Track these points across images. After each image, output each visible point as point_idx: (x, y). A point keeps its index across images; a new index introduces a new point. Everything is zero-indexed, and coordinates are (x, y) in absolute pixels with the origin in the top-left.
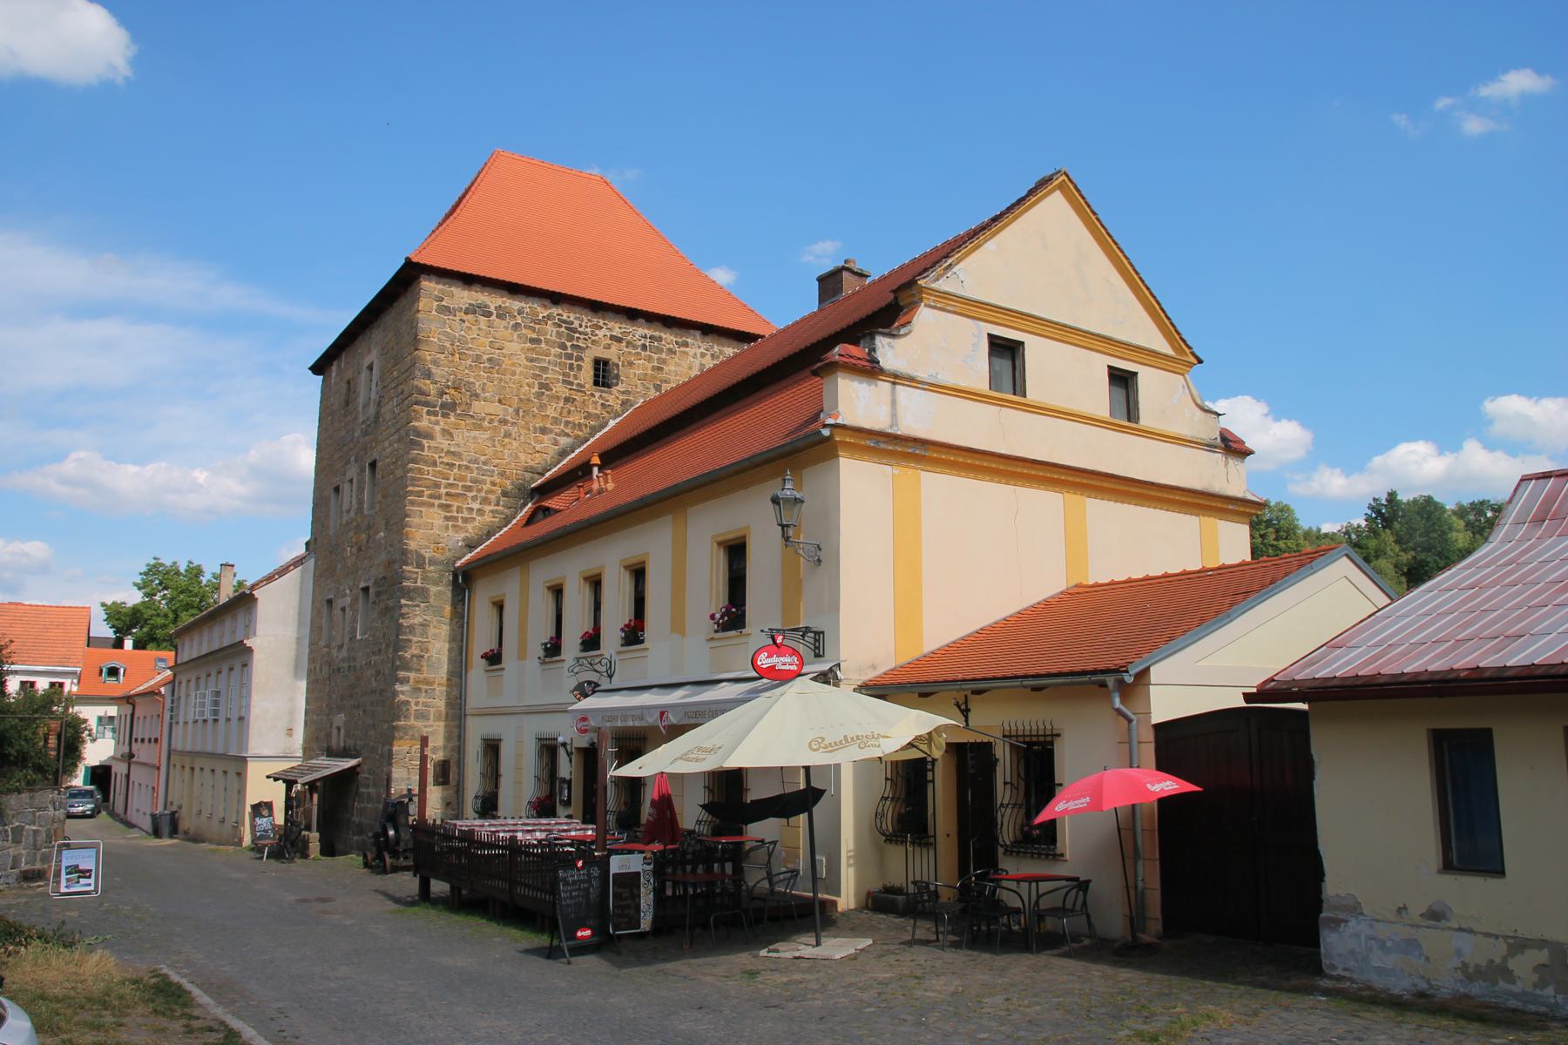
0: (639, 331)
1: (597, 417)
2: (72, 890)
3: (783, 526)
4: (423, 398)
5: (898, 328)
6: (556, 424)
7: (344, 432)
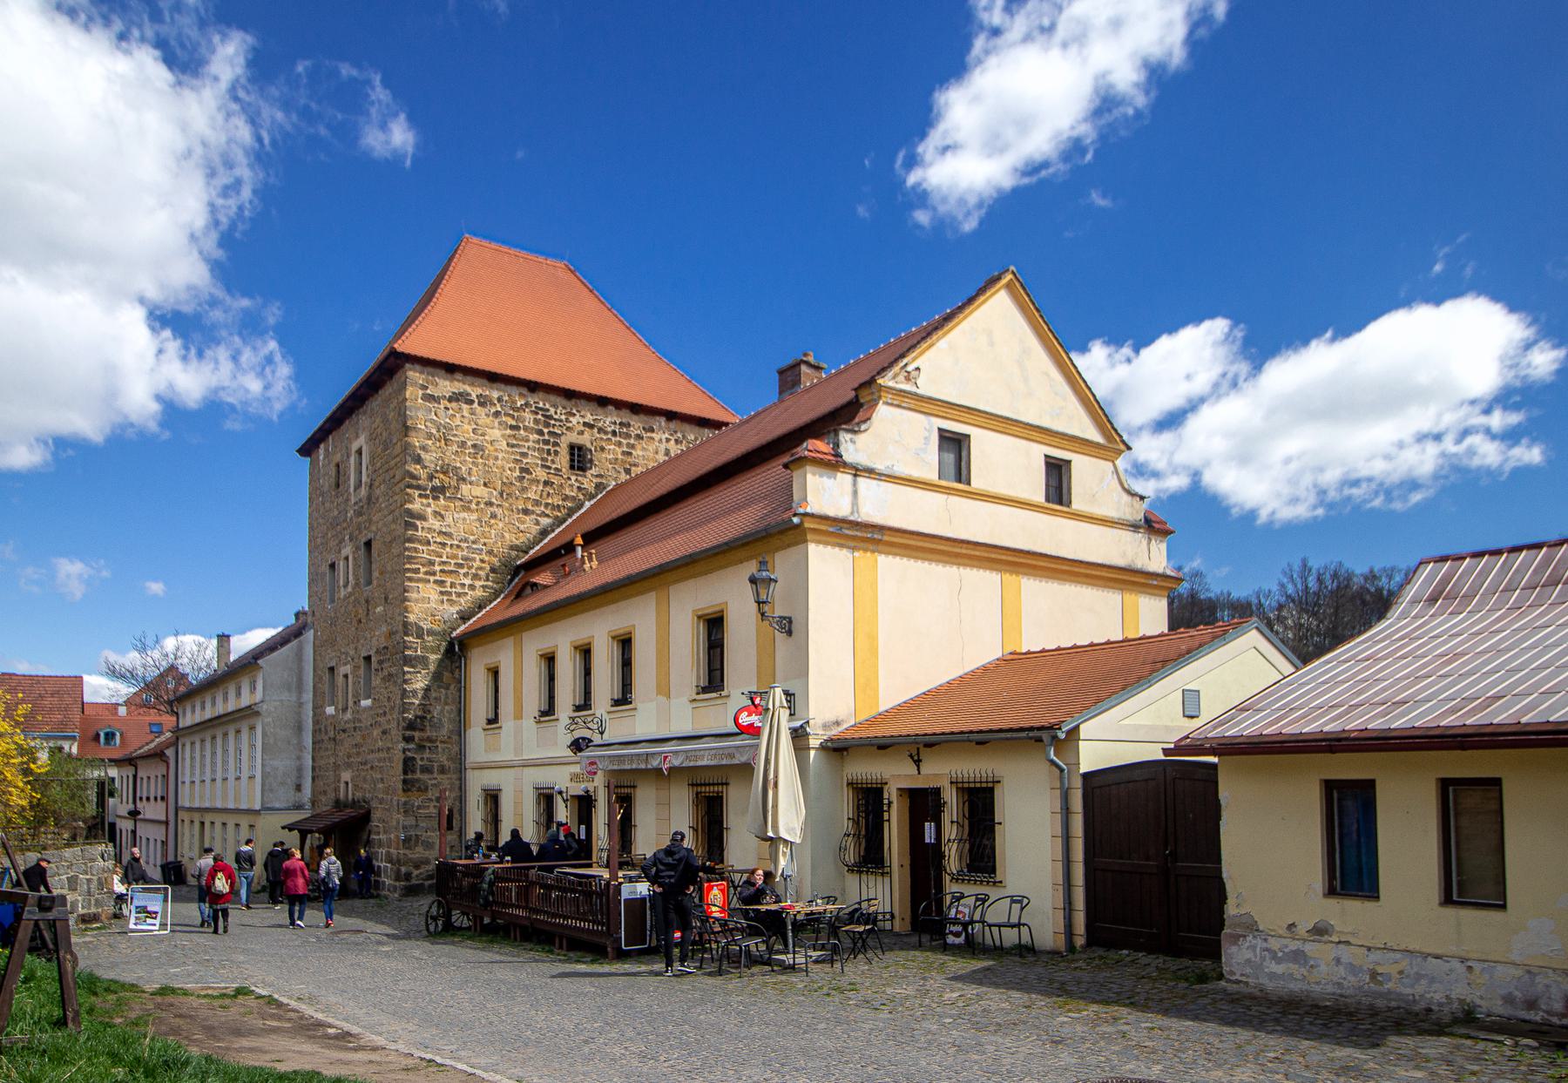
0: (609, 419)
1: (574, 498)
2: (140, 927)
3: (759, 603)
4: (414, 482)
5: (858, 424)
6: (537, 505)
7: (336, 513)
